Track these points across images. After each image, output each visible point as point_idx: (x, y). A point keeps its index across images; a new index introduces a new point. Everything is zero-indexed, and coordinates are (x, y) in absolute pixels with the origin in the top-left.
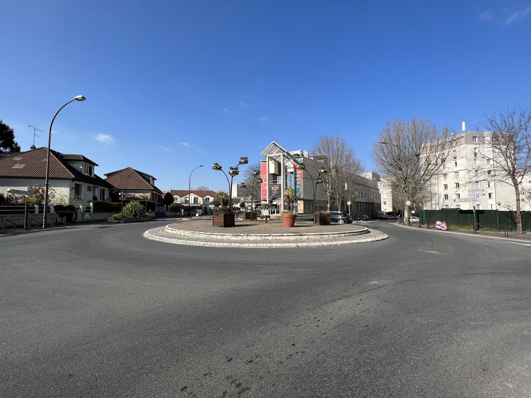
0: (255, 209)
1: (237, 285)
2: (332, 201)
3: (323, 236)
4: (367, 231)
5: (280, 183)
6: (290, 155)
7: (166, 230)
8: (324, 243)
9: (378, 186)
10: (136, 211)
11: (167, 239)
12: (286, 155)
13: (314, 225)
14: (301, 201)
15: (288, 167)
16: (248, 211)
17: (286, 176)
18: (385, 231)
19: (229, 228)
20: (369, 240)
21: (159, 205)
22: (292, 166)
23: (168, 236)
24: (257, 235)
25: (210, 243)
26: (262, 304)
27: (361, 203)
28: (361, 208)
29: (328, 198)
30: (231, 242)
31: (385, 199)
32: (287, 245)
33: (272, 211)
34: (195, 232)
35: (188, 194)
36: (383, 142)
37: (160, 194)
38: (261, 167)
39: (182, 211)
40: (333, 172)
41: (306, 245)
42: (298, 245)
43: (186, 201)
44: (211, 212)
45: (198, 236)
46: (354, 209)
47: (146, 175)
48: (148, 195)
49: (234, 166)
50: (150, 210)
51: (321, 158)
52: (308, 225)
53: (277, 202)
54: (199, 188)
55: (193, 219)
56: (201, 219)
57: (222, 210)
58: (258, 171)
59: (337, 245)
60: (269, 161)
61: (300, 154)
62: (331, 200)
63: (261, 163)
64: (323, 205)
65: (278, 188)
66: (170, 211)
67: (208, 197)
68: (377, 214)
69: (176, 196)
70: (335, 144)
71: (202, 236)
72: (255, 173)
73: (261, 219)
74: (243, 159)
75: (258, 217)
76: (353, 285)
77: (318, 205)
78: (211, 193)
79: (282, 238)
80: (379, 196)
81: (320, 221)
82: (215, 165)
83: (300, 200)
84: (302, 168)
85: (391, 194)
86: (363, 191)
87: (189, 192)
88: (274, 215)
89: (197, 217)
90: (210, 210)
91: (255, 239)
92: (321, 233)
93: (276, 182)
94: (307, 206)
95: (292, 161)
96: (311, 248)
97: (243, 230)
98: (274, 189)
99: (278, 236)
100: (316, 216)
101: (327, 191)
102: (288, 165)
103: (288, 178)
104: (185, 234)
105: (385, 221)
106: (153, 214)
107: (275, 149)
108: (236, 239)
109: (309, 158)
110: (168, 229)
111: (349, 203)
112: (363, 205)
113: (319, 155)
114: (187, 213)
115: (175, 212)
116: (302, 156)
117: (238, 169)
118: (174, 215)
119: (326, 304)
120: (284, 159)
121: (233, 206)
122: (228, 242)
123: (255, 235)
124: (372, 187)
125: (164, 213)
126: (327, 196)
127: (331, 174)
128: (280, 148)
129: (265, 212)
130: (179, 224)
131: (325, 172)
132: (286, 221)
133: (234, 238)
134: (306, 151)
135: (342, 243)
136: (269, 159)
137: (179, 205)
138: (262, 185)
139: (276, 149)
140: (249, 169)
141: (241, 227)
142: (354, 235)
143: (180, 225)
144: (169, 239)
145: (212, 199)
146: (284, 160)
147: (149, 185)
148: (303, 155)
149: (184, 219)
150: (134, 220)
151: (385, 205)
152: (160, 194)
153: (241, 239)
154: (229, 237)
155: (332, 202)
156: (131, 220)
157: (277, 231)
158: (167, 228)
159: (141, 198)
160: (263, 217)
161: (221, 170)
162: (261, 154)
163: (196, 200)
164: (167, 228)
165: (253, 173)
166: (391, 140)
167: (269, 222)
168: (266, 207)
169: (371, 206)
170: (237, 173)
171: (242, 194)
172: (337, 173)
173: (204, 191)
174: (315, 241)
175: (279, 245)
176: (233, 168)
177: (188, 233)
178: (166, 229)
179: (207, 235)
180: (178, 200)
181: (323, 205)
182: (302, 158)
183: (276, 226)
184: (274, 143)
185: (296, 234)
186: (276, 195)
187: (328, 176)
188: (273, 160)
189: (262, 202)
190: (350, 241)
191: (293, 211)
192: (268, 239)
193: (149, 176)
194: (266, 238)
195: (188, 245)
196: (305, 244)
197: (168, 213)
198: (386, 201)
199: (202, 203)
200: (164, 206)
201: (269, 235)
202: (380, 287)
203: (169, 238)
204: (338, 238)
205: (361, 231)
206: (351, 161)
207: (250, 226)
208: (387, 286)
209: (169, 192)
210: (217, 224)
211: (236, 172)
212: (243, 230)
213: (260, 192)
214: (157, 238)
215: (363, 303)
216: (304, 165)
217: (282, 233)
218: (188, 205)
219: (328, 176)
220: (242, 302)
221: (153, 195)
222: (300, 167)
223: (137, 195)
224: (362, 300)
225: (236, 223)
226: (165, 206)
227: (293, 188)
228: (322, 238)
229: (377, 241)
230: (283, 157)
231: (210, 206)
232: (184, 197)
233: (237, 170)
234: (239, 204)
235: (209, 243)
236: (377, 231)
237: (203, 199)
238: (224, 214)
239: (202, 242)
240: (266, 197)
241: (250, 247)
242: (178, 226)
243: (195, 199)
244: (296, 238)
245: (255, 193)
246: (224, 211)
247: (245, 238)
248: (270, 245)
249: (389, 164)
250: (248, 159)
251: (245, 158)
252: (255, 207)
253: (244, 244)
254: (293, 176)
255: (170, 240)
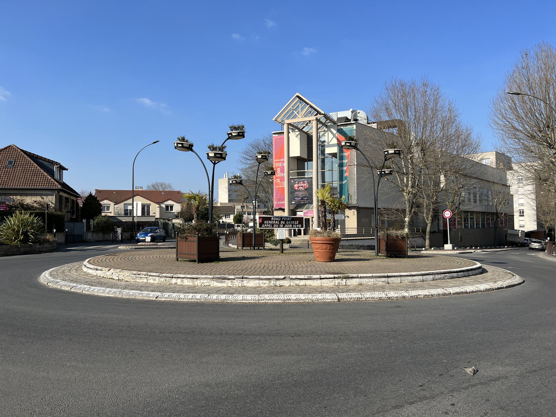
0: (260, 227)
1: (215, 375)
2: (413, 210)
3: (390, 279)
4: (480, 270)
5: (311, 176)
6: (332, 121)
7: (85, 269)
8: (391, 293)
9: (506, 180)
10: (27, 231)
11: (85, 286)
12: (323, 120)
13: (375, 257)
14: (353, 210)
15: (326, 144)
16: (249, 230)
17: (323, 161)
18: (516, 269)
19: (209, 264)
20: (483, 287)
21: (72, 220)
22: (335, 141)
23: (87, 280)
24: (262, 277)
25: (168, 294)
26: (260, 413)
27: (472, 213)
28: (474, 224)
29: (405, 203)
30: (209, 291)
31: (522, 205)
32: (319, 296)
33: (295, 230)
34: (139, 273)
35: (130, 198)
36: (515, 91)
37: (74, 199)
38: (274, 143)
39: (119, 230)
40: (417, 153)
41: (355, 297)
42: (340, 297)
43: (126, 210)
44: (179, 231)
45: (145, 281)
46: (458, 225)
47: (45, 159)
48: (51, 200)
49: (218, 144)
50: (55, 230)
51: (392, 124)
52: (362, 257)
53: (304, 213)
54: (153, 186)
55: (139, 247)
56: (156, 247)
57: (195, 229)
58: (265, 153)
59: (416, 297)
60: (289, 132)
61: (350, 118)
62: (412, 209)
63: (274, 135)
64: (396, 218)
65: (306, 185)
66: (93, 231)
67: (170, 202)
68: (506, 235)
69: (106, 202)
70: (419, 96)
71: (154, 280)
72: (259, 157)
73: (273, 247)
74: (235, 128)
75: (267, 241)
76: (440, 375)
77: (386, 219)
78: (177, 196)
79: (308, 282)
80: (509, 200)
81: (387, 250)
82: (180, 140)
83: (350, 208)
84: (350, 146)
85: (533, 196)
86: (477, 189)
87: (133, 194)
88: (299, 239)
89: (148, 242)
90: (173, 228)
91: (258, 285)
92: (386, 274)
93: (303, 174)
94: (363, 220)
95: (335, 132)
96: (366, 303)
97: (235, 268)
98: (298, 188)
99: (301, 279)
100: (379, 241)
101: (404, 191)
102: (327, 141)
103: (327, 167)
104: (121, 277)
105: (521, 248)
106: (60, 238)
107: (300, 109)
108: (219, 285)
109: (368, 125)
110: (88, 267)
111: (447, 214)
112: (477, 218)
113: (387, 119)
114: (127, 235)
115: (104, 233)
116: (354, 122)
117: (225, 150)
118: (100, 239)
119: (383, 412)
120: (320, 128)
121: (221, 221)
122: (204, 292)
123: (258, 277)
124: (495, 181)
125: (81, 236)
126: (403, 199)
127: (411, 157)
128: (311, 107)
129: (281, 233)
130: (110, 257)
131: (397, 153)
132: (319, 251)
133: (216, 284)
134: (361, 112)
135: (428, 294)
136: (288, 128)
137: (112, 220)
138: (276, 180)
139: (302, 109)
140: (251, 148)
141: (232, 263)
142: (452, 278)
143: (111, 260)
144: (89, 287)
145: (177, 208)
146: (318, 129)
147: (52, 179)
148: (356, 120)
149: (121, 247)
150: (22, 250)
151: (522, 218)
152: (74, 199)
153: (230, 285)
154: (206, 282)
155: (414, 212)
156: (15, 250)
157: (300, 269)
158: (85, 266)
159: (37, 206)
160: (276, 242)
161: (192, 150)
162: (274, 119)
163: (145, 209)
164: (85, 266)
165: (257, 156)
166: (530, 88)
167: (288, 252)
168: (283, 222)
169: (493, 220)
170: (224, 156)
171: (237, 197)
172: (424, 155)
173: (162, 192)
174: (374, 288)
175: (302, 296)
176: (215, 146)
177: (126, 276)
178: (83, 267)
179: (162, 279)
180: (111, 209)
181: (396, 218)
182: (355, 126)
183: (298, 260)
184: (298, 97)
185: (336, 276)
186: (302, 199)
187: (406, 160)
188: (297, 130)
189: (277, 214)
190: (443, 290)
191: (334, 230)
192: (282, 286)
193: (52, 163)
194: (278, 283)
195: (126, 299)
196: (354, 295)
197: (90, 236)
198: (523, 210)
199: (158, 216)
200: (82, 222)
201: (284, 278)
202: (492, 381)
203: (89, 284)
204: (419, 283)
205: (468, 270)
206: (452, 131)
207: (249, 261)
208: (507, 378)
209: (93, 195)
210: (184, 256)
211: (221, 154)
212: (235, 268)
213: (272, 193)
214: (65, 286)
215: (456, 412)
216: (356, 141)
217: (310, 273)
218: (129, 219)
219: (406, 160)
220: (222, 409)
221: (60, 199)
222: (347, 144)
223: (29, 200)
224: (454, 405)
225: (222, 255)
226: (84, 221)
227: (336, 184)
228: (388, 283)
229: (498, 289)
230: (317, 124)
231: (174, 221)
232: (122, 204)
233: (222, 151)
234: (232, 217)
235: (166, 295)
236: (500, 270)
237: (161, 207)
238: (199, 237)
239: (153, 293)
240: (283, 202)
241: (247, 302)
242: (107, 261)
243: (143, 207)
244: (336, 284)
245: (263, 195)
246: (199, 231)
247: (237, 283)
248: (286, 298)
249: (528, 136)
250: (246, 130)
251: (239, 127)
252: (260, 223)
253: (236, 295)
254: (336, 161)
255: (92, 289)
